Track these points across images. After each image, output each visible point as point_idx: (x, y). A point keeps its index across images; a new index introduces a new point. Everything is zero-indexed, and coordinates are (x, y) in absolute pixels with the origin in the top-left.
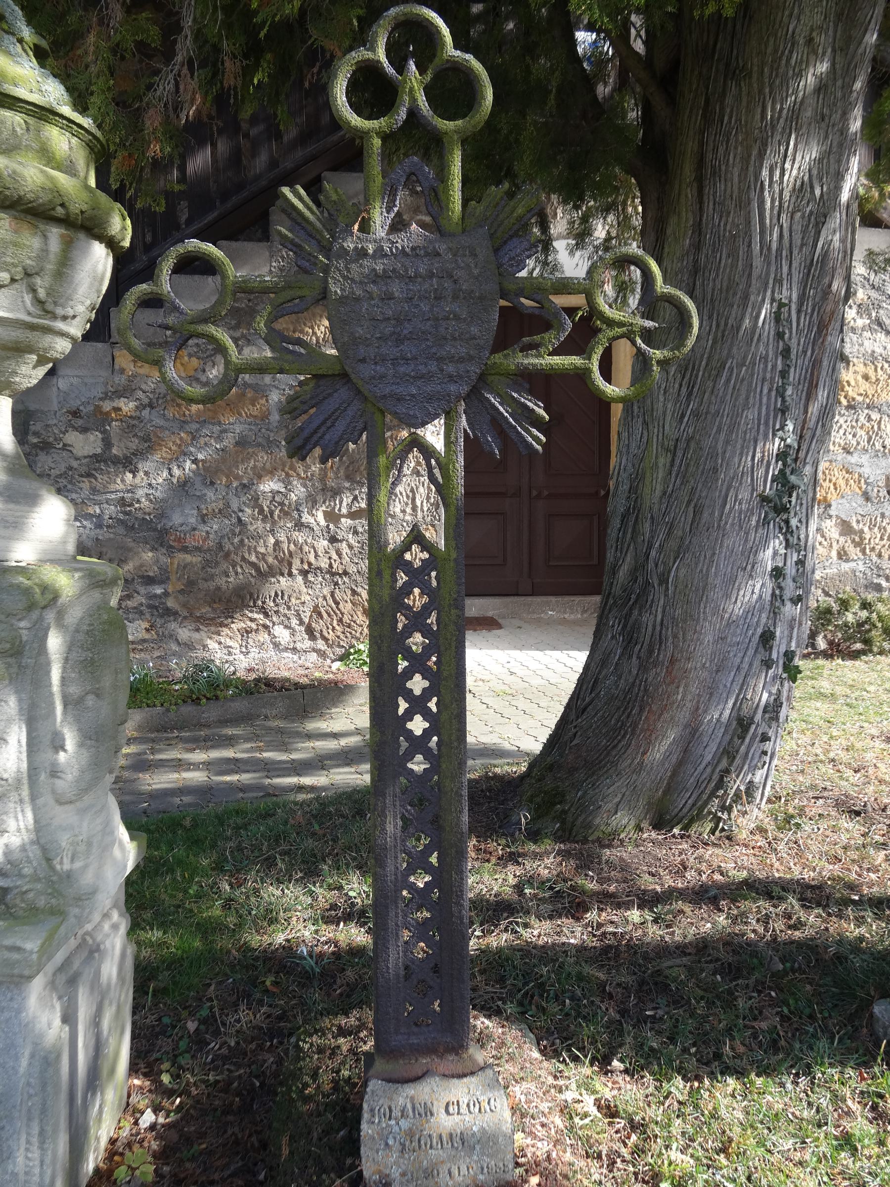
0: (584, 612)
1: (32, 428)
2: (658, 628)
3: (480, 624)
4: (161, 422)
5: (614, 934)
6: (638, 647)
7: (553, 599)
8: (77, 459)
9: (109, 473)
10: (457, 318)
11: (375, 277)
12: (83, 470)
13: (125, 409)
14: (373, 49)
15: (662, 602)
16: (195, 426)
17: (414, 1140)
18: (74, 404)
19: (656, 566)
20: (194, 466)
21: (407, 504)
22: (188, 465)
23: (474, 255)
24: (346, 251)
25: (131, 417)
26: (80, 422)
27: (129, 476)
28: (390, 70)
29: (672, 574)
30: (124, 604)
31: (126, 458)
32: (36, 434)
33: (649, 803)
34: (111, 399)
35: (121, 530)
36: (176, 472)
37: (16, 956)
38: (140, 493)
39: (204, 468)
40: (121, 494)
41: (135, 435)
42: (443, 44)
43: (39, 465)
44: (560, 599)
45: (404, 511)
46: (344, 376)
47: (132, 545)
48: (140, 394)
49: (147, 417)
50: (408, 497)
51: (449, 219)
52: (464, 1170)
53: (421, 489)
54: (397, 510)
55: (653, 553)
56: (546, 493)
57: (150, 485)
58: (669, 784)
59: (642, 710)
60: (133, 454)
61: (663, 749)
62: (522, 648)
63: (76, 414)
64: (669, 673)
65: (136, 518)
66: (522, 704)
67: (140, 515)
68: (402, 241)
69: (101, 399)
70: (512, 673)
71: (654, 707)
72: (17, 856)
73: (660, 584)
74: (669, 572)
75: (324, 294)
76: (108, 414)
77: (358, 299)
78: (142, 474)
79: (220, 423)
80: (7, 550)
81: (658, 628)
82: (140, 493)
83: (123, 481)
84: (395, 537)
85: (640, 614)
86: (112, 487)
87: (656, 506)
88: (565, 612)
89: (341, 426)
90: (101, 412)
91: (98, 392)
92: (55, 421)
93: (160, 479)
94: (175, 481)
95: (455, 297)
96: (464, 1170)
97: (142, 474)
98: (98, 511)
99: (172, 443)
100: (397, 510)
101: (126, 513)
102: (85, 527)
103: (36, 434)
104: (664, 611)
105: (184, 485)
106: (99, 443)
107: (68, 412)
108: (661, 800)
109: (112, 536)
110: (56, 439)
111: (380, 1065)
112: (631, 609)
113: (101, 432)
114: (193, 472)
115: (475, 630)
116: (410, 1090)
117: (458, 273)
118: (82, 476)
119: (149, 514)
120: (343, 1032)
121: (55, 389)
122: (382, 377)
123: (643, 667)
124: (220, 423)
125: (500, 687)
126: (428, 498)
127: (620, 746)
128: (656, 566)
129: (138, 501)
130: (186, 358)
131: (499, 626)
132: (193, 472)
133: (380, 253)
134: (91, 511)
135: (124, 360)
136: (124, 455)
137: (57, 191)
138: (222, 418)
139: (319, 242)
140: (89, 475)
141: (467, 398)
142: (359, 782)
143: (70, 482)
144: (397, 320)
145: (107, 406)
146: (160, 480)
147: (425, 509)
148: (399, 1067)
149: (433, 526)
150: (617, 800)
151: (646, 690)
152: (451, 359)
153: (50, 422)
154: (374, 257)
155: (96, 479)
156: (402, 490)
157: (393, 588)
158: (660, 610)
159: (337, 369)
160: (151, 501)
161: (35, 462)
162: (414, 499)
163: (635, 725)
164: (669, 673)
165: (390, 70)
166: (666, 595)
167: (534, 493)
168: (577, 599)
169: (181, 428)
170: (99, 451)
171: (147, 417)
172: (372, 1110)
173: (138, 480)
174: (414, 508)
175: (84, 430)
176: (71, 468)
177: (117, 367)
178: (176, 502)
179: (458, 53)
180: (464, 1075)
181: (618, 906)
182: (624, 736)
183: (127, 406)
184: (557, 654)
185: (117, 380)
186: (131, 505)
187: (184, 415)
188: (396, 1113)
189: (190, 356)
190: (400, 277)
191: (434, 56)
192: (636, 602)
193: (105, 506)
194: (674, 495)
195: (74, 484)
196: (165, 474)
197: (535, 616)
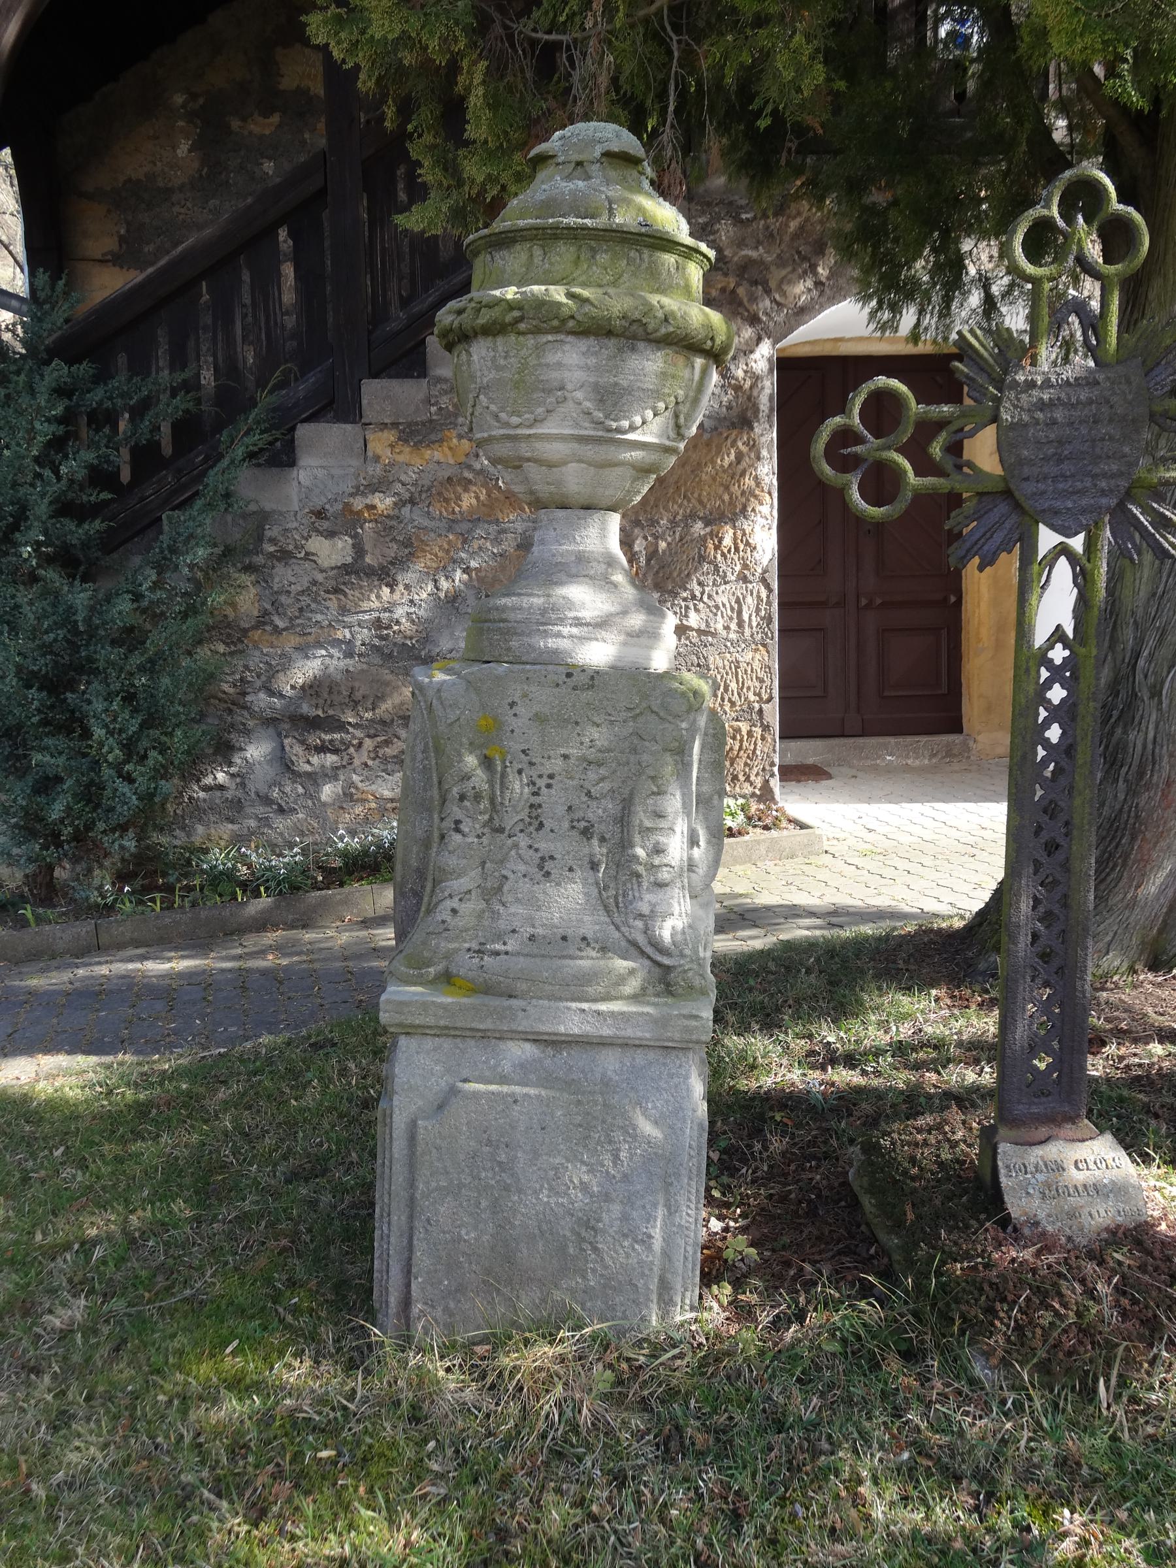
0: (933, 756)
1: (268, 534)
2: (1150, 746)
3: (803, 774)
4: (426, 522)
5: (1140, 1065)
6: (1124, 769)
7: (892, 740)
8: (322, 571)
9: (361, 587)
10: (1111, 439)
11: (1042, 405)
12: (331, 584)
13: (381, 506)
14: (1048, 206)
15: (1154, 717)
16: (465, 526)
17: (1053, 1190)
18: (318, 502)
19: (1146, 677)
20: (465, 576)
21: (731, 619)
22: (458, 575)
23: (1129, 382)
24: (1016, 383)
25: (388, 517)
26: (326, 525)
27: (386, 590)
28: (1061, 223)
29: (1167, 685)
30: (381, 752)
31: (383, 568)
32: (273, 541)
33: (1143, 943)
34: (364, 494)
35: (377, 660)
36: (444, 584)
37: (694, 1023)
38: (400, 612)
39: (479, 579)
40: (377, 614)
41: (394, 540)
42: (1109, 200)
43: (277, 580)
44: (900, 739)
45: (727, 628)
46: (1007, 494)
47: (390, 677)
48: (398, 487)
49: (408, 515)
50: (732, 609)
51: (1107, 351)
52: (1103, 1213)
53: (749, 599)
54: (720, 626)
55: (1141, 662)
56: (879, 601)
57: (411, 601)
58: (1164, 921)
59: (1133, 838)
60: (392, 563)
61: (1158, 882)
62: (870, 800)
63: (320, 514)
64: (1164, 796)
65: (395, 644)
66: (902, 865)
67: (399, 639)
68: (1068, 373)
69: (352, 495)
70: (870, 831)
71: (1148, 835)
72: (679, 937)
73: (1152, 697)
74: (1163, 683)
75: (995, 419)
76: (359, 513)
77: (1026, 425)
78: (401, 587)
79: (497, 522)
80: (649, 659)
81: (1150, 746)
82: (400, 612)
83: (378, 597)
84: (1040, 637)
85: (1125, 732)
86: (365, 605)
87: (1141, 609)
88: (907, 757)
89: (998, 537)
90: (351, 512)
91: (348, 486)
92: (295, 524)
93: (424, 594)
94: (442, 595)
95: (1111, 421)
96: (1103, 1213)
97: (401, 587)
98: (348, 636)
99: (437, 546)
100: (720, 626)
101: (382, 638)
102: (331, 657)
103: (273, 541)
104: (1157, 727)
105: (453, 600)
106: (349, 550)
107: (312, 512)
108: (1156, 940)
109: (365, 667)
110: (296, 547)
111: (1003, 1131)
112: (1113, 727)
113: (351, 537)
114: (465, 584)
115: (799, 781)
116: (1038, 1152)
117: (1114, 399)
118: (328, 592)
119: (411, 638)
120: (920, 1131)
121: (295, 483)
122: (1043, 493)
123: (1132, 792)
124: (497, 522)
125: (863, 847)
126: (758, 610)
127: (1109, 879)
128: (1146, 677)
129: (398, 623)
130: (455, 441)
131: (829, 776)
132: (465, 584)
133: (1047, 384)
134: (339, 635)
135: (381, 443)
136: (380, 564)
137: (709, 327)
138: (500, 516)
139: (989, 375)
140: (336, 591)
141: (1113, 512)
142: (739, 950)
143: (315, 600)
144: (1059, 442)
145: (358, 503)
146: (424, 596)
147: (754, 624)
148: (1023, 1133)
149: (764, 645)
150: (1109, 938)
151: (1137, 817)
152: (1104, 475)
153: (289, 526)
154: (1041, 388)
155: (345, 595)
156: (726, 601)
157: (1037, 682)
158: (1151, 726)
159: (1001, 487)
160: (413, 622)
161: (271, 575)
162: (740, 613)
163: (1126, 856)
164: (1164, 796)
165: (1061, 223)
166: (1159, 709)
167: (864, 602)
168: (924, 739)
169: (450, 529)
170: (349, 560)
171: (408, 515)
172: (1008, 1167)
173: (397, 596)
174: (740, 624)
175: (331, 534)
176: (314, 583)
177: (370, 454)
178: (444, 622)
179: (1121, 207)
180: (1083, 1141)
181: (1135, 1041)
182: (1113, 869)
183: (383, 503)
184: (917, 807)
185: (370, 470)
186: (389, 627)
187: (453, 512)
188: (1031, 1168)
189: (460, 437)
190: (1064, 404)
191: (1101, 209)
192: (1119, 718)
193: (357, 629)
194: (1166, 597)
195: (319, 603)
196: (430, 587)
197: (869, 762)
